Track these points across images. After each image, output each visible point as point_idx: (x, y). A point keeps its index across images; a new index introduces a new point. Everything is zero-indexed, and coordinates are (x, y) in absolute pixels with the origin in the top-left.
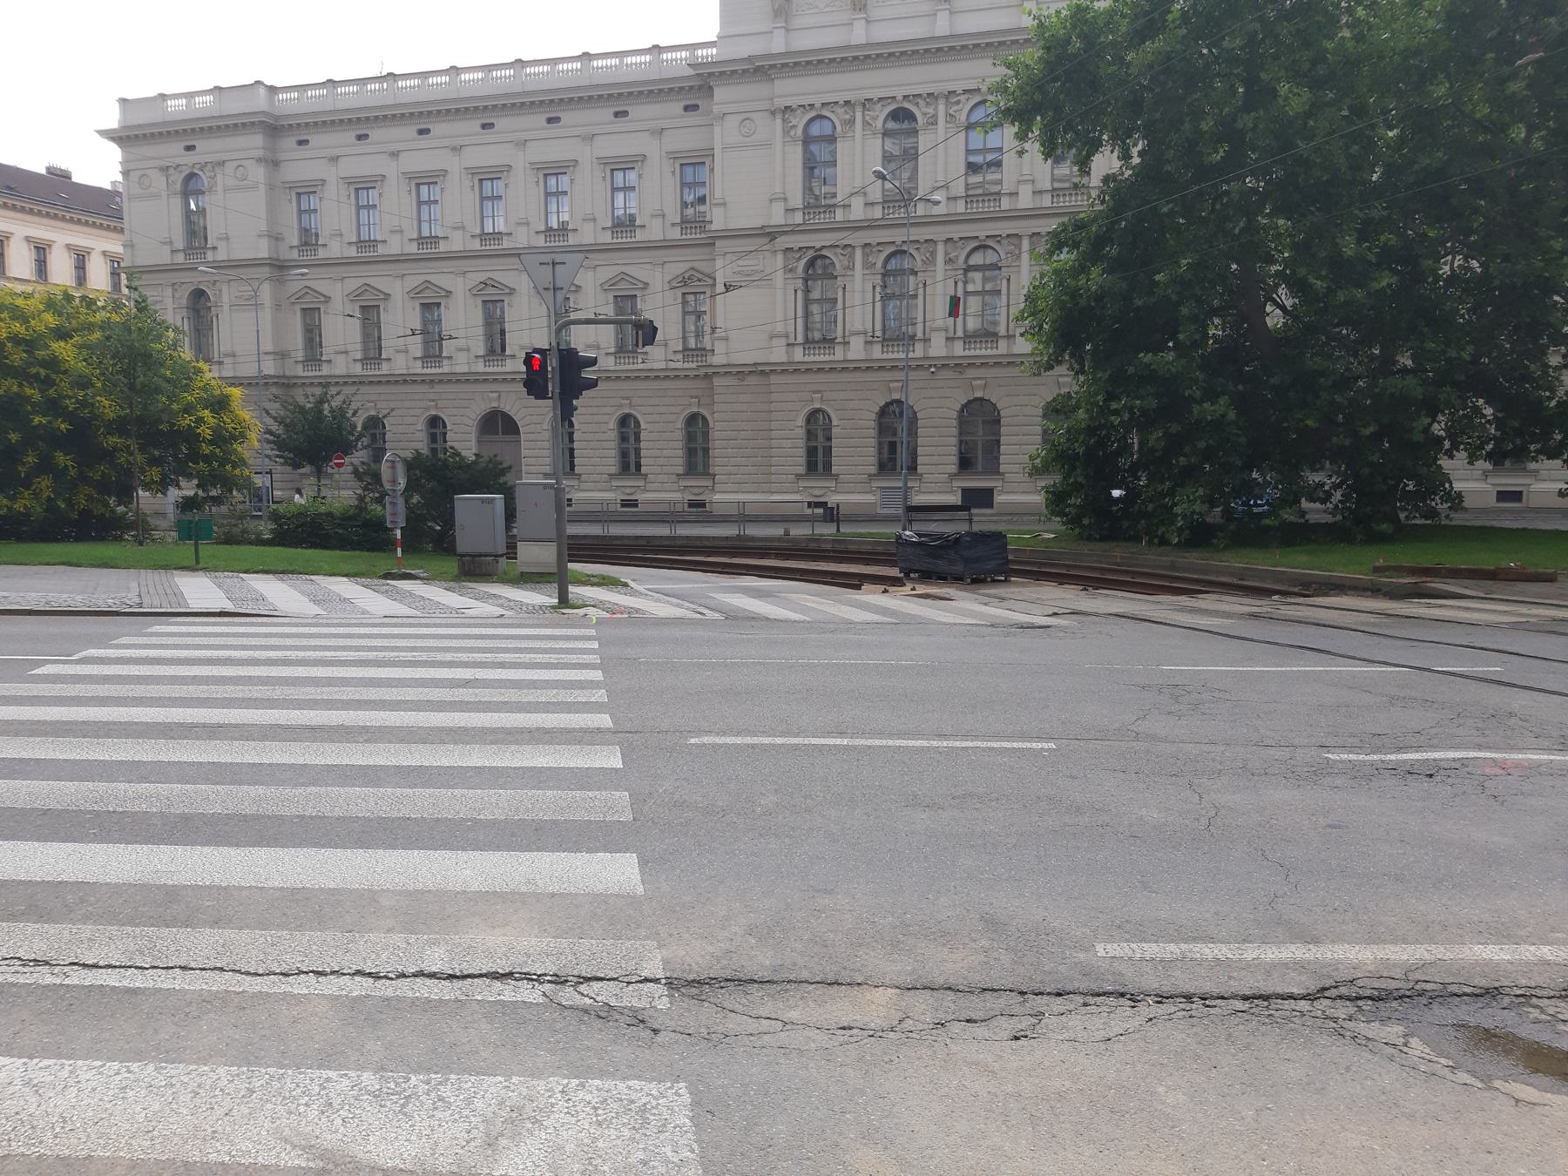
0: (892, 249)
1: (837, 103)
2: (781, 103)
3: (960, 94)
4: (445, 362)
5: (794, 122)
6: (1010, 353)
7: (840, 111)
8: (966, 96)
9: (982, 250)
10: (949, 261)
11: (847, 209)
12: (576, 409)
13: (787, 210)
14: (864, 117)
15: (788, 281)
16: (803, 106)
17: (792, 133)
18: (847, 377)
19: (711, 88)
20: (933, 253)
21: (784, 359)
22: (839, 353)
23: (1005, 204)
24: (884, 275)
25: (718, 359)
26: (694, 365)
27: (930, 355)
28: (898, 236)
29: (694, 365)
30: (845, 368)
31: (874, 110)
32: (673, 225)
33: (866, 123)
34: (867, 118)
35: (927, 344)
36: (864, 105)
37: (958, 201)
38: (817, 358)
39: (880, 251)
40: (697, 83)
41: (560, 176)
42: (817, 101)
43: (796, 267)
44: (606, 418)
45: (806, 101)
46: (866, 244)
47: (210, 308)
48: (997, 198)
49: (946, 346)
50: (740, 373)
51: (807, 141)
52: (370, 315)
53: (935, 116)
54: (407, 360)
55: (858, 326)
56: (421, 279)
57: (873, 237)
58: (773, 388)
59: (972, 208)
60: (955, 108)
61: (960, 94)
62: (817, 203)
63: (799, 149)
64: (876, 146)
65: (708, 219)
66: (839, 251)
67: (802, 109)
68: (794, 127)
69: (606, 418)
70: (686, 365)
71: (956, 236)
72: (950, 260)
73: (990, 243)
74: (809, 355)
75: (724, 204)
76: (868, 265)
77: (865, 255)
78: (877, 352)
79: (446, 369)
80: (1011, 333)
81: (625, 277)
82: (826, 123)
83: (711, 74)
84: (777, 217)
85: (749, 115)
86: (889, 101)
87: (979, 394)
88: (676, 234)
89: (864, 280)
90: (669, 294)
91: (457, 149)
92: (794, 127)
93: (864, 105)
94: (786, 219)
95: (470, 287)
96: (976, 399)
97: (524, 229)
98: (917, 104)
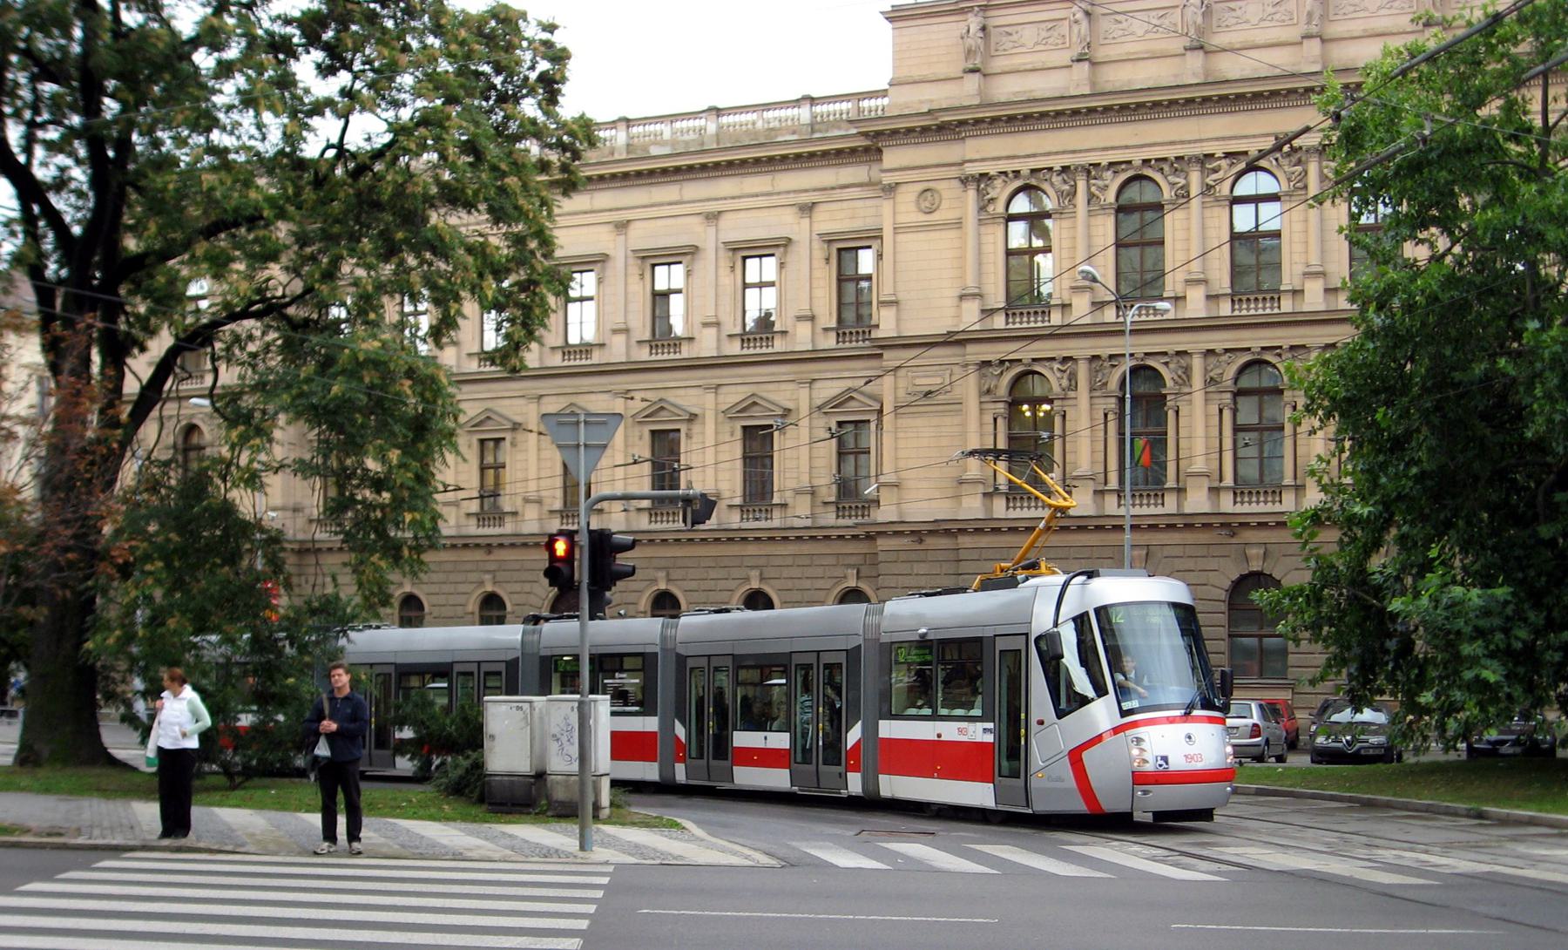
1: (1050, 169)
2: (973, 169)
3: (1220, 158)
4: (776, 513)
5: (992, 194)
6: (519, 532)
7: (1056, 179)
9: (1257, 367)
10: (1210, 381)
11: (1298, 297)
16: (1005, 173)
17: (990, 208)
18: (791, 549)
19: (879, 151)
20: (1187, 370)
22: (1170, 504)
25: (885, 513)
26: (852, 521)
29: (852, 521)
30: (1189, 524)
31: (1101, 178)
32: (826, 330)
33: (1091, 197)
35: (1182, 495)
36: (1089, 172)
37: (1221, 299)
38: (1254, 508)
39: (1114, 366)
40: (862, 142)
41: (764, 259)
42: (1137, 157)
44: (462, 599)
46: (1208, 351)
47: (1165, 396)
48: (1276, 296)
50: (919, 533)
51: (1122, 210)
53: (1186, 187)
54: (812, 506)
55: (1199, 465)
56: (748, 390)
58: (963, 555)
59: (1240, 310)
60: (1215, 176)
61: (1220, 158)
63: (1110, 222)
64: (1105, 229)
65: (873, 322)
66: (1056, 366)
67: (1003, 177)
68: (992, 200)
69: (462, 599)
70: (841, 522)
71: (1218, 347)
72: (1212, 379)
73: (1268, 357)
75: (896, 303)
76: (1095, 388)
77: (1093, 374)
78: (999, 508)
79: (776, 523)
81: (759, 401)
83: (878, 134)
84: (969, 317)
85: (931, 185)
86: (1123, 166)
90: (727, 427)
91: (713, 217)
92: (992, 200)
93: (1089, 172)
94: (1208, 309)
97: (713, 331)
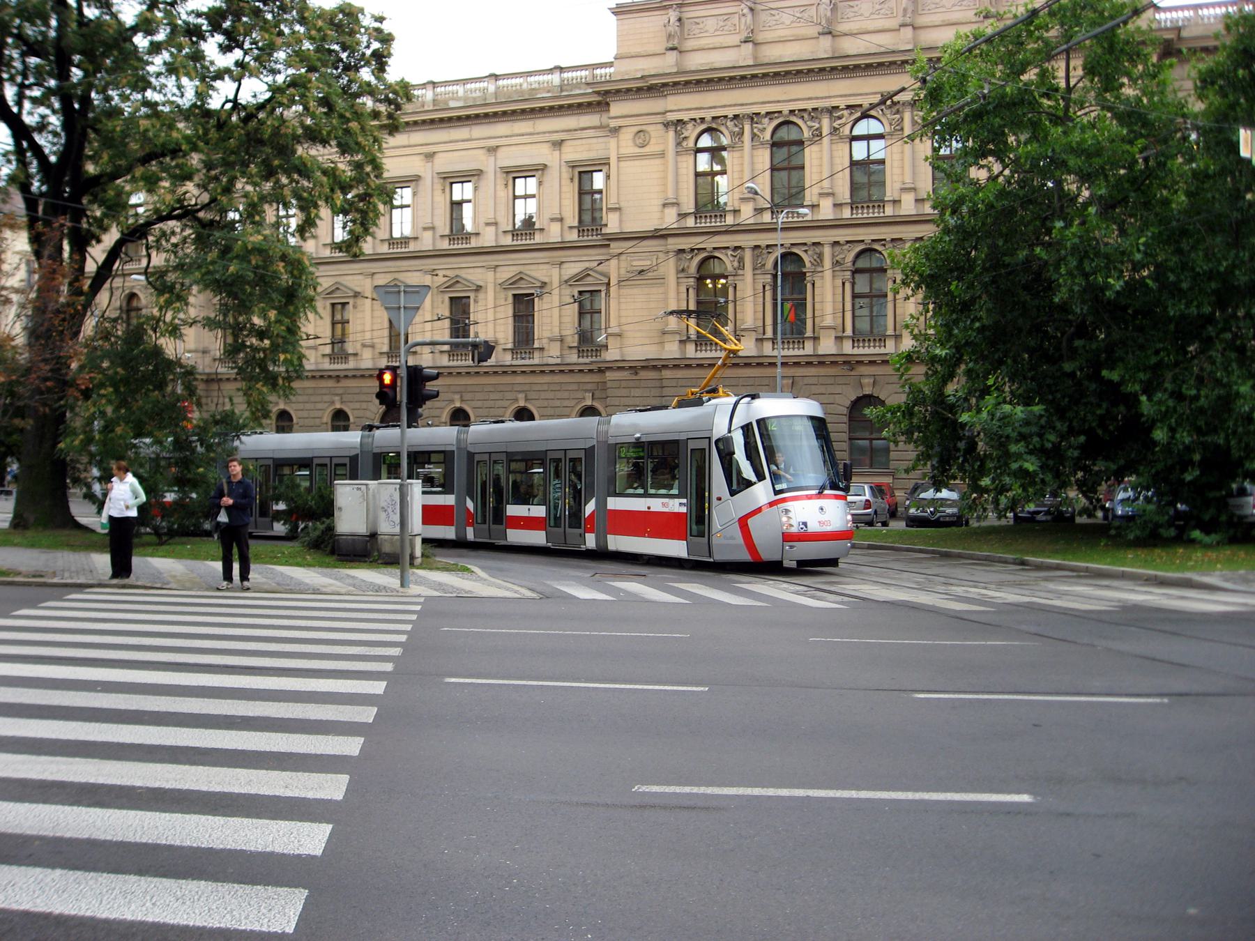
0: (861, 247)
3: (843, 109)
4: (536, 354)
5: (686, 134)
8: (848, 111)
9: (868, 254)
10: (836, 263)
11: (897, 205)
12: (421, 416)
13: (679, 215)
14: (752, 129)
15: (680, 280)
16: (694, 120)
17: (684, 144)
19: (608, 104)
20: (820, 256)
21: (834, 351)
22: (809, 348)
23: (889, 210)
24: (856, 272)
25: (612, 354)
27: (820, 353)
28: (867, 235)
30: (822, 361)
32: (571, 228)
33: (754, 136)
34: (755, 130)
42: (786, 108)
43: (688, 267)
45: (697, 115)
49: (756, 346)
50: (636, 368)
52: (524, 307)
53: (819, 129)
55: (828, 321)
57: (764, 239)
59: (857, 214)
61: (843, 109)
62: (707, 205)
66: (730, 252)
68: (685, 138)
70: (581, 360)
71: (842, 239)
73: (876, 246)
74: (858, 347)
75: (619, 209)
77: (755, 258)
79: (536, 361)
80: (897, 333)
82: (794, 129)
83: (607, 92)
84: (670, 219)
87: (867, 391)
88: (573, 236)
89: (834, 276)
93: (752, 119)
95: (501, 281)
96: (865, 396)
97: (493, 228)
98: (802, 117)
